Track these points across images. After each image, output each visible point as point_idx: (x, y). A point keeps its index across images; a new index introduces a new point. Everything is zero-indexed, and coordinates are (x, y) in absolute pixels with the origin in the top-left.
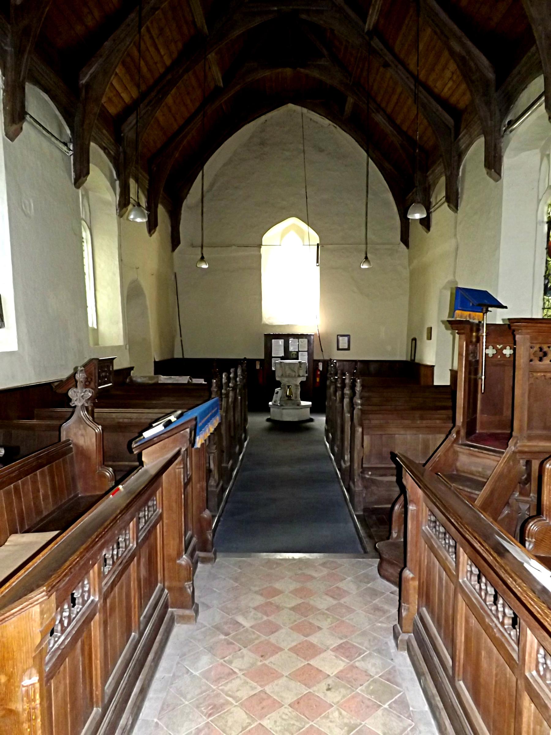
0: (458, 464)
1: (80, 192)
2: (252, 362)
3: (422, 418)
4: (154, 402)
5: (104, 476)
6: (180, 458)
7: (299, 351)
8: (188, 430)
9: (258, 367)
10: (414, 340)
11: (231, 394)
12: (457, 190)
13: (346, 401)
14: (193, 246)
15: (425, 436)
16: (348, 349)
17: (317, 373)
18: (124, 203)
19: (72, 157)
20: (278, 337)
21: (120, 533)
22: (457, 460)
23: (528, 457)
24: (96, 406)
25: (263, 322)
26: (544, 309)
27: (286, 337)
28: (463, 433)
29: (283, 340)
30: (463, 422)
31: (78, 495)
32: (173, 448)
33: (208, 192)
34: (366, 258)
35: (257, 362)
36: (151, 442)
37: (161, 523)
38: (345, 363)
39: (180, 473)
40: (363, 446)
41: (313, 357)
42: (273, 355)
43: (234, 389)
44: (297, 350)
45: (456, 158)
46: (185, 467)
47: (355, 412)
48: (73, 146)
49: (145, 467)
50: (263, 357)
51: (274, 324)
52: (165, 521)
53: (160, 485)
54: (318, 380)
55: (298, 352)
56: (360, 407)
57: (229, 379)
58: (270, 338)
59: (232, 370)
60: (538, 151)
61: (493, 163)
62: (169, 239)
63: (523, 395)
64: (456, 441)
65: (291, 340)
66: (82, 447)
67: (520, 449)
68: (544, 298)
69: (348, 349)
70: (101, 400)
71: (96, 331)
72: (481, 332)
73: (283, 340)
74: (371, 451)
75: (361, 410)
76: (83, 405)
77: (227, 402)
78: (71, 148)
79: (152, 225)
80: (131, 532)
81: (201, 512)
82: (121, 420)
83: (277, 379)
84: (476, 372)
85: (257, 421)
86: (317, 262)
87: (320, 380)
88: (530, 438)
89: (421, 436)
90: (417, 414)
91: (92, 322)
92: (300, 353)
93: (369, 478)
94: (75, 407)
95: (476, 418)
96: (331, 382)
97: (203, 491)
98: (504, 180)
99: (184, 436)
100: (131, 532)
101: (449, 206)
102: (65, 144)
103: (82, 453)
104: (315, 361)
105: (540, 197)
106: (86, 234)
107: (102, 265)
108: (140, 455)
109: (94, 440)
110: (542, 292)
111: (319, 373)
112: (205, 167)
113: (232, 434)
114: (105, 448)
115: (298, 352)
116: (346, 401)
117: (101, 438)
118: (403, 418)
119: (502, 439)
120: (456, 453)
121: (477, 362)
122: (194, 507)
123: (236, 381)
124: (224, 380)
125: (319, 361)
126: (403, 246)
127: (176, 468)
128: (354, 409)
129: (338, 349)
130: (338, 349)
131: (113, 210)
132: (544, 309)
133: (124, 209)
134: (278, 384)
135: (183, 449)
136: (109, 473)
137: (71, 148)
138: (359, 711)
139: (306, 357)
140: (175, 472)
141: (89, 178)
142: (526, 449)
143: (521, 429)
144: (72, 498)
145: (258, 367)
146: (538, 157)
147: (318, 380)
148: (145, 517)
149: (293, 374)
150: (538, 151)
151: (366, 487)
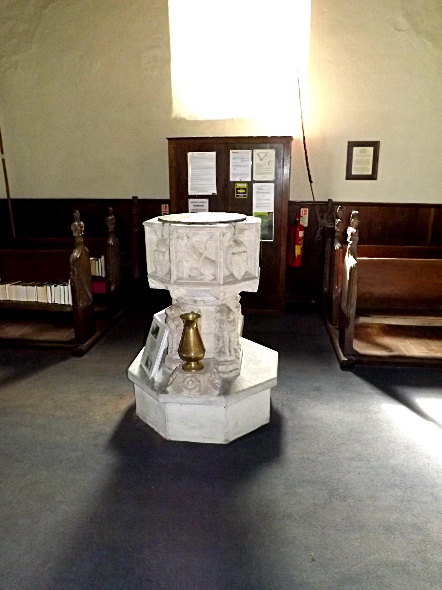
7: (253, 181)
16: (373, 177)
17: (296, 234)
20: (202, 144)
25: (174, 115)
27: (223, 147)
41: (287, 195)
42: (190, 193)
44: (249, 179)
51: (198, 119)
54: (298, 250)
55: (250, 184)
58: (181, 148)
65: (234, 155)
83: (153, 284)
87: (303, 250)
92: (255, 185)
104: (291, 203)
111: (301, 234)
115: (250, 184)
125: (303, 204)
130: (350, 176)
134: (163, 299)
138: (301, 518)
139: (271, 197)
147: (298, 250)
149: (208, 273)
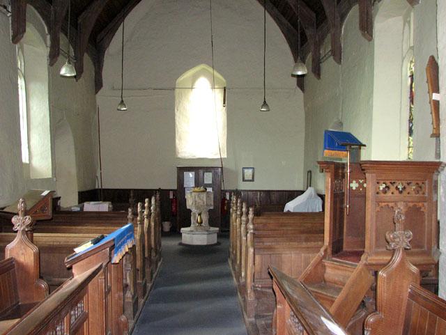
0: (326, 276)
1: (17, 46)
2: (163, 193)
3: (307, 240)
4: (80, 227)
5: (41, 288)
6: (102, 270)
8: (108, 249)
9: (171, 197)
10: (310, 172)
11: (146, 221)
12: (341, 47)
13: (243, 226)
14: (113, 89)
15: (307, 255)
16: (253, 180)
18: (54, 56)
19: (10, 18)
20: (190, 169)
21: (58, 324)
22: (325, 272)
23: (375, 268)
24: (33, 231)
26: (409, 147)
28: (329, 251)
29: (194, 173)
30: (329, 243)
31: (18, 302)
32: (96, 264)
33: (127, 41)
34: (265, 104)
35: (171, 192)
36: (80, 258)
37: (87, 321)
38: (249, 193)
39: (101, 283)
40: (254, 264)
43: (149, 215)
45: (339, 19)
46: (106, 278)
47: (248, 235)
48: (12, 8)
49: (75, 278)
50: (175, 188)
52: (91, 320)
53: (87, 292)
56: (252, 231)
57: (143, 207)
58: (182, 170)
59: (147, 200)
60: (401, 17)
61: (366, 27)
62: (93, 83)
63: (371, 219)
64: (324, 257)
66: (22, 264)
67: (370, 262)
68: (409, 139)
69: (253, 180)
70: (38, 225)
71: (29, 166)
72: (346, 170)
73: (194, 173)
74: (261, 268)
75: (254, 234)
76: (23, 230)
77: (142, 227)
78: (10, 10)
79: (79, 70)
80: (65, 324)
81: (119, 316)
82: (52, 243)
83: (188, 207)
84: (342, 202)
85: (169, 243)
86: (224, 103)
88: (377, 254)
89: (303, 255)
90: (303, 236)
91: (25, 159)
93: (260, 291)
94: (17, 232)
95: (342, 239)
96: (233, 210)
97: (120, 299)
98: (375, 43)
99: (105, 254)
100: (65, 324)
101: (334, 59)
102: (5, 7)
103: (22, 267)
105: (404, 55)
106: (21, 82)
107: (35, 108)
108: (70, 268)
109: (32, 258)
110: (408, 134)
112: (125, 21)
113: (146, 255)
114: (42, 264)
116: (243, 226)
117: (38, 257)
118: (291, 240)
119: (357, 255)
120: (324, 267)
121: (343, 193)
122: (113, 309)
123: (150, 210)
124: (139, 209)
125: (226, 191)
126: (299, 89)
127: (99, 279)
128: (247, 233)
129: (244, 180)
130: (244, 180)
131: (45, 61)
132: (409, 147)
133: (55, 60)
135: (104, 264)
136: (43, 285)
137: (10, 10)
140: (98, 282)
141: (25, 35)
142: (374, 262)
143: (370, 248)
144: (15, 305)
145: (171, 197)
146: (402, 23)
148: (75, 315)
150: (401, 17)
151: (258, 298)
